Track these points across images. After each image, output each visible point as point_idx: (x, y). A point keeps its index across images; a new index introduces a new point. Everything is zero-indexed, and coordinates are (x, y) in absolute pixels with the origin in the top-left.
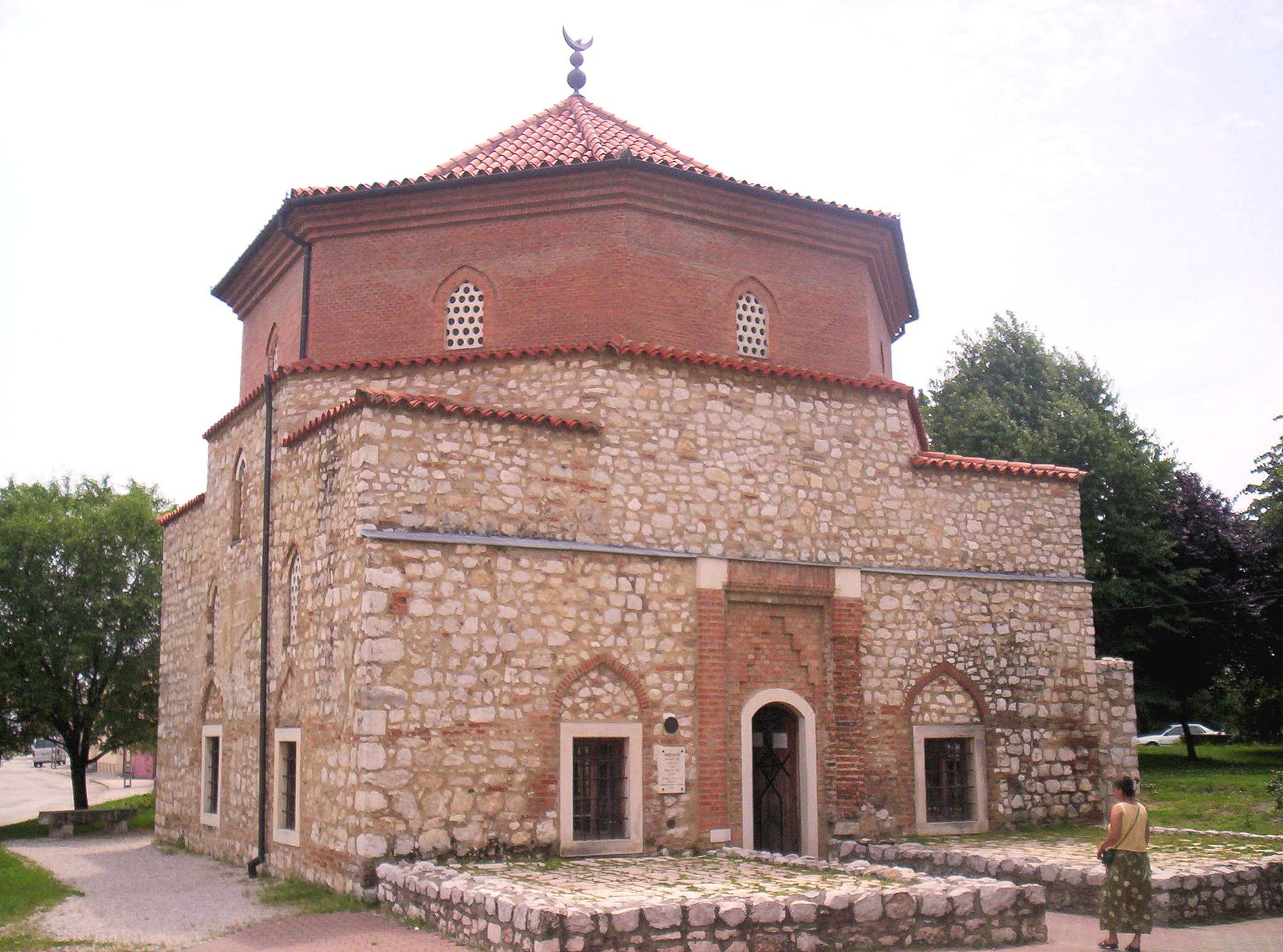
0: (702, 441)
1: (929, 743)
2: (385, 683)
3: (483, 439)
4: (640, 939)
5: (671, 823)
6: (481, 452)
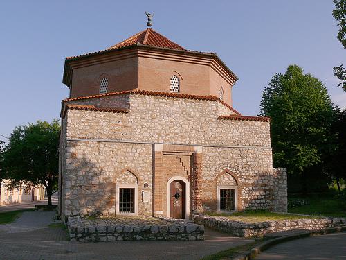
0: (158, 114)
1: (222, 191)
2: (71, 174)
3: (98, 115)
4: (95, 235)
5: (146, 209)
6: (98, 119)
